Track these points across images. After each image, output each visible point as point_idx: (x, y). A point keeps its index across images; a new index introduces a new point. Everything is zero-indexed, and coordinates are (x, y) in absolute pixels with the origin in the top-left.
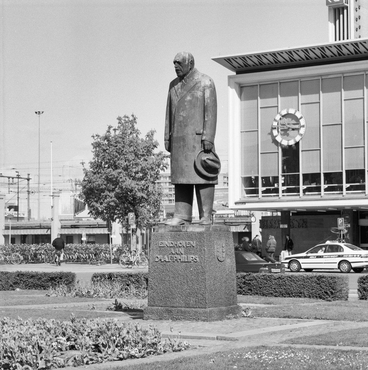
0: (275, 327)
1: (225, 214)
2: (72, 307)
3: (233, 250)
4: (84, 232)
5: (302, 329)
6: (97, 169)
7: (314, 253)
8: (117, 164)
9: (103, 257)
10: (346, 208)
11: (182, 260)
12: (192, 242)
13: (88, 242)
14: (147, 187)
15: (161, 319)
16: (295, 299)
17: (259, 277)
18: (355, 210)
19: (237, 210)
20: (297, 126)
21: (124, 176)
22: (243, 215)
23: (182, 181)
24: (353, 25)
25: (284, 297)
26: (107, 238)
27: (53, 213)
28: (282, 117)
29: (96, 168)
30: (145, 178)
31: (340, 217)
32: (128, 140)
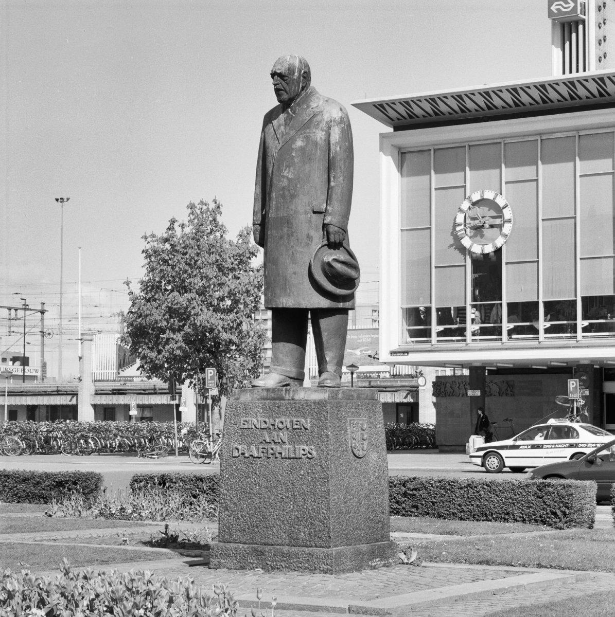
0: (463, 585)
1: (374, 372)
2: (87, 538)
3: (383, 436)
4: (133, 401)
5: (515, 589)
6: (153, 293)
7: (528, 440)
8: (186, 284)
9: (164, 444)
10: (582, 362)
11: (283, 454)
12: (303, 420)
13: (142, 419)
14: (240, 324)
15: (243, 568)
16: (497, 524)
17: (432, 484)
18: (598, 367)
19: (394, 364)
20: (498, 221)
21: (198, 305)
22: (404, 374)
23: (284, 301)
24: (593, 51)
25: (478, 520)
26: (171, 412)
27: (81, 369)
28: (471, 206)
29: (151, 291)
30: (235, 308)
31: (572, 378)
32: (207, 242)
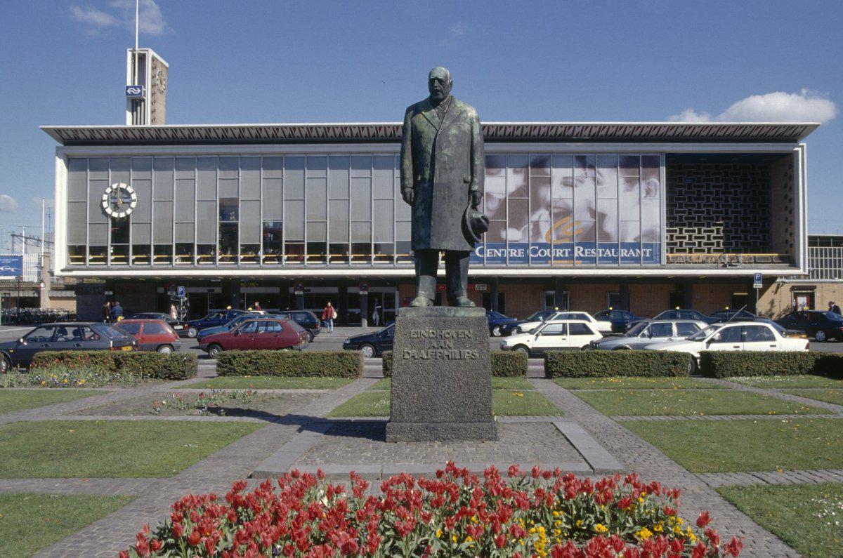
12: (467, 332)
15: (417, 440)
